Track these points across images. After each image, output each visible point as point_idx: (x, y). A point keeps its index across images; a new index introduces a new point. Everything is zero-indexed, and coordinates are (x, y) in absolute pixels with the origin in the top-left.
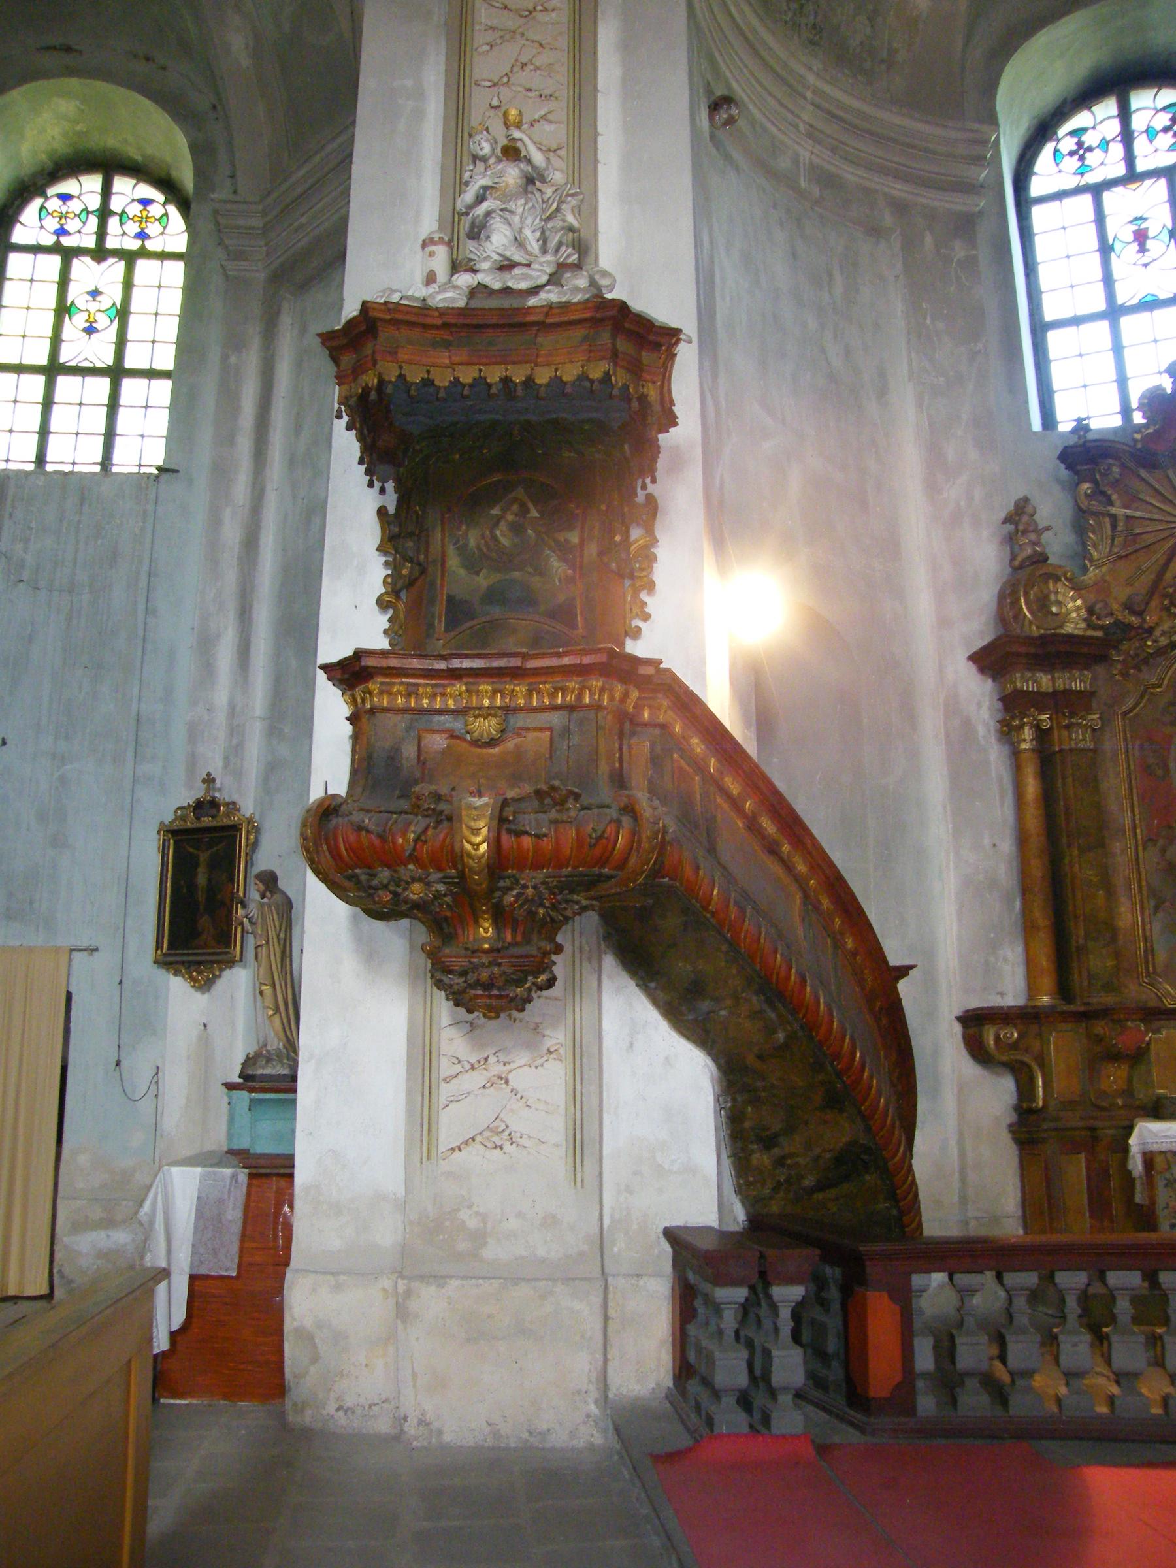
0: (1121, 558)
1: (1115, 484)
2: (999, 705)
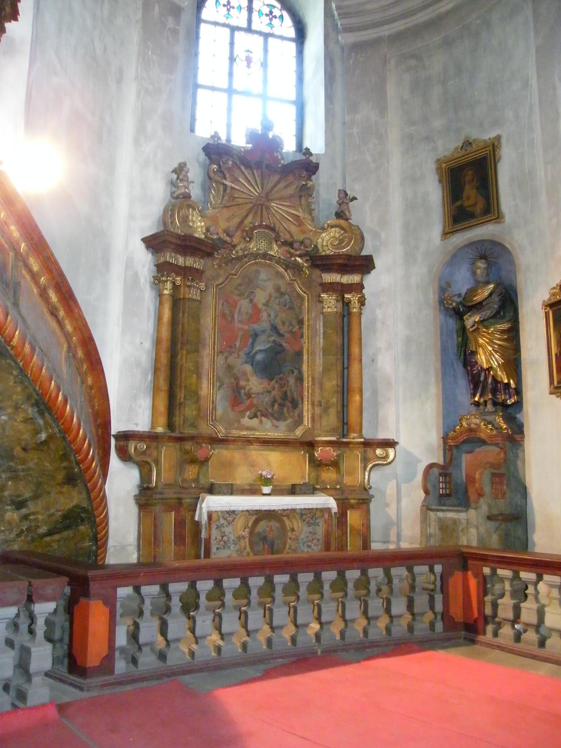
0: (226, 207)
1: (229, 169)
2: (154, 269)
